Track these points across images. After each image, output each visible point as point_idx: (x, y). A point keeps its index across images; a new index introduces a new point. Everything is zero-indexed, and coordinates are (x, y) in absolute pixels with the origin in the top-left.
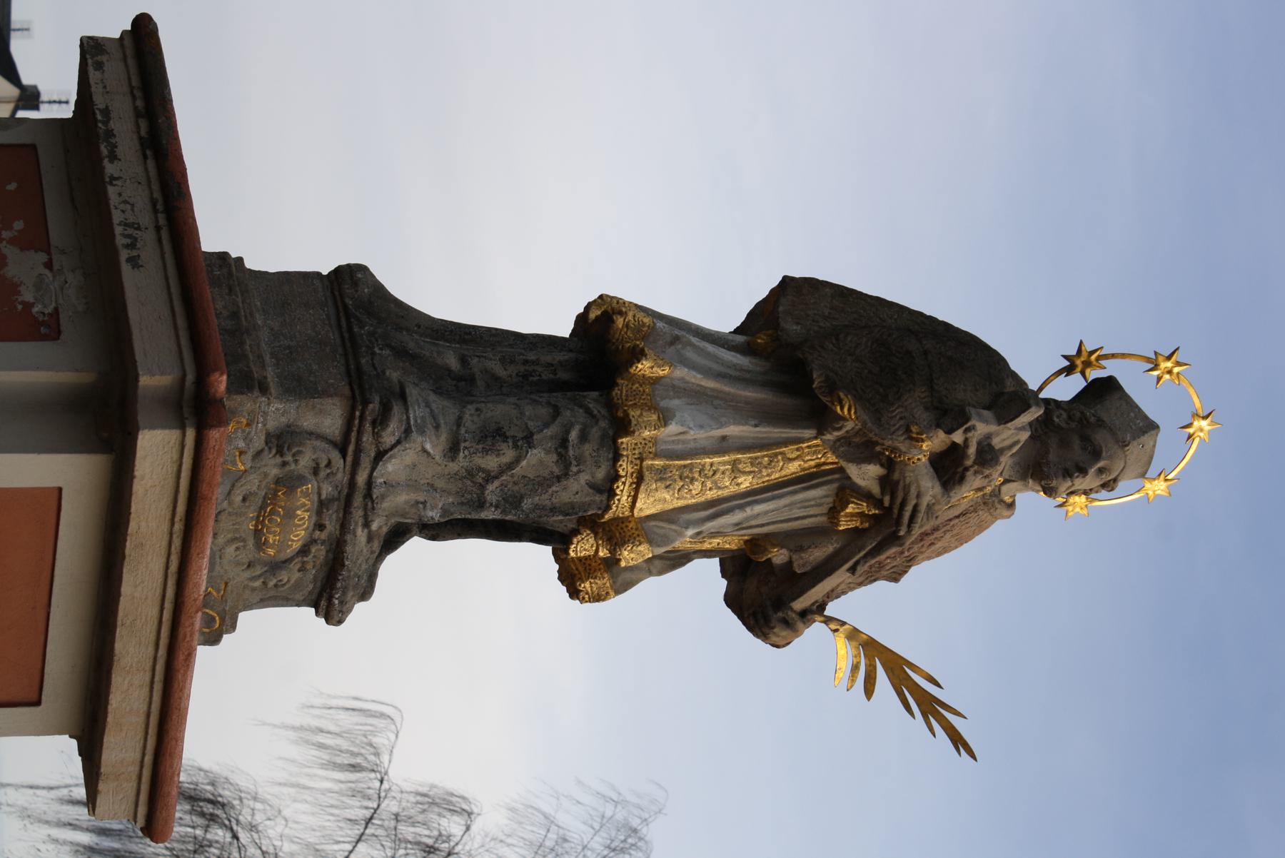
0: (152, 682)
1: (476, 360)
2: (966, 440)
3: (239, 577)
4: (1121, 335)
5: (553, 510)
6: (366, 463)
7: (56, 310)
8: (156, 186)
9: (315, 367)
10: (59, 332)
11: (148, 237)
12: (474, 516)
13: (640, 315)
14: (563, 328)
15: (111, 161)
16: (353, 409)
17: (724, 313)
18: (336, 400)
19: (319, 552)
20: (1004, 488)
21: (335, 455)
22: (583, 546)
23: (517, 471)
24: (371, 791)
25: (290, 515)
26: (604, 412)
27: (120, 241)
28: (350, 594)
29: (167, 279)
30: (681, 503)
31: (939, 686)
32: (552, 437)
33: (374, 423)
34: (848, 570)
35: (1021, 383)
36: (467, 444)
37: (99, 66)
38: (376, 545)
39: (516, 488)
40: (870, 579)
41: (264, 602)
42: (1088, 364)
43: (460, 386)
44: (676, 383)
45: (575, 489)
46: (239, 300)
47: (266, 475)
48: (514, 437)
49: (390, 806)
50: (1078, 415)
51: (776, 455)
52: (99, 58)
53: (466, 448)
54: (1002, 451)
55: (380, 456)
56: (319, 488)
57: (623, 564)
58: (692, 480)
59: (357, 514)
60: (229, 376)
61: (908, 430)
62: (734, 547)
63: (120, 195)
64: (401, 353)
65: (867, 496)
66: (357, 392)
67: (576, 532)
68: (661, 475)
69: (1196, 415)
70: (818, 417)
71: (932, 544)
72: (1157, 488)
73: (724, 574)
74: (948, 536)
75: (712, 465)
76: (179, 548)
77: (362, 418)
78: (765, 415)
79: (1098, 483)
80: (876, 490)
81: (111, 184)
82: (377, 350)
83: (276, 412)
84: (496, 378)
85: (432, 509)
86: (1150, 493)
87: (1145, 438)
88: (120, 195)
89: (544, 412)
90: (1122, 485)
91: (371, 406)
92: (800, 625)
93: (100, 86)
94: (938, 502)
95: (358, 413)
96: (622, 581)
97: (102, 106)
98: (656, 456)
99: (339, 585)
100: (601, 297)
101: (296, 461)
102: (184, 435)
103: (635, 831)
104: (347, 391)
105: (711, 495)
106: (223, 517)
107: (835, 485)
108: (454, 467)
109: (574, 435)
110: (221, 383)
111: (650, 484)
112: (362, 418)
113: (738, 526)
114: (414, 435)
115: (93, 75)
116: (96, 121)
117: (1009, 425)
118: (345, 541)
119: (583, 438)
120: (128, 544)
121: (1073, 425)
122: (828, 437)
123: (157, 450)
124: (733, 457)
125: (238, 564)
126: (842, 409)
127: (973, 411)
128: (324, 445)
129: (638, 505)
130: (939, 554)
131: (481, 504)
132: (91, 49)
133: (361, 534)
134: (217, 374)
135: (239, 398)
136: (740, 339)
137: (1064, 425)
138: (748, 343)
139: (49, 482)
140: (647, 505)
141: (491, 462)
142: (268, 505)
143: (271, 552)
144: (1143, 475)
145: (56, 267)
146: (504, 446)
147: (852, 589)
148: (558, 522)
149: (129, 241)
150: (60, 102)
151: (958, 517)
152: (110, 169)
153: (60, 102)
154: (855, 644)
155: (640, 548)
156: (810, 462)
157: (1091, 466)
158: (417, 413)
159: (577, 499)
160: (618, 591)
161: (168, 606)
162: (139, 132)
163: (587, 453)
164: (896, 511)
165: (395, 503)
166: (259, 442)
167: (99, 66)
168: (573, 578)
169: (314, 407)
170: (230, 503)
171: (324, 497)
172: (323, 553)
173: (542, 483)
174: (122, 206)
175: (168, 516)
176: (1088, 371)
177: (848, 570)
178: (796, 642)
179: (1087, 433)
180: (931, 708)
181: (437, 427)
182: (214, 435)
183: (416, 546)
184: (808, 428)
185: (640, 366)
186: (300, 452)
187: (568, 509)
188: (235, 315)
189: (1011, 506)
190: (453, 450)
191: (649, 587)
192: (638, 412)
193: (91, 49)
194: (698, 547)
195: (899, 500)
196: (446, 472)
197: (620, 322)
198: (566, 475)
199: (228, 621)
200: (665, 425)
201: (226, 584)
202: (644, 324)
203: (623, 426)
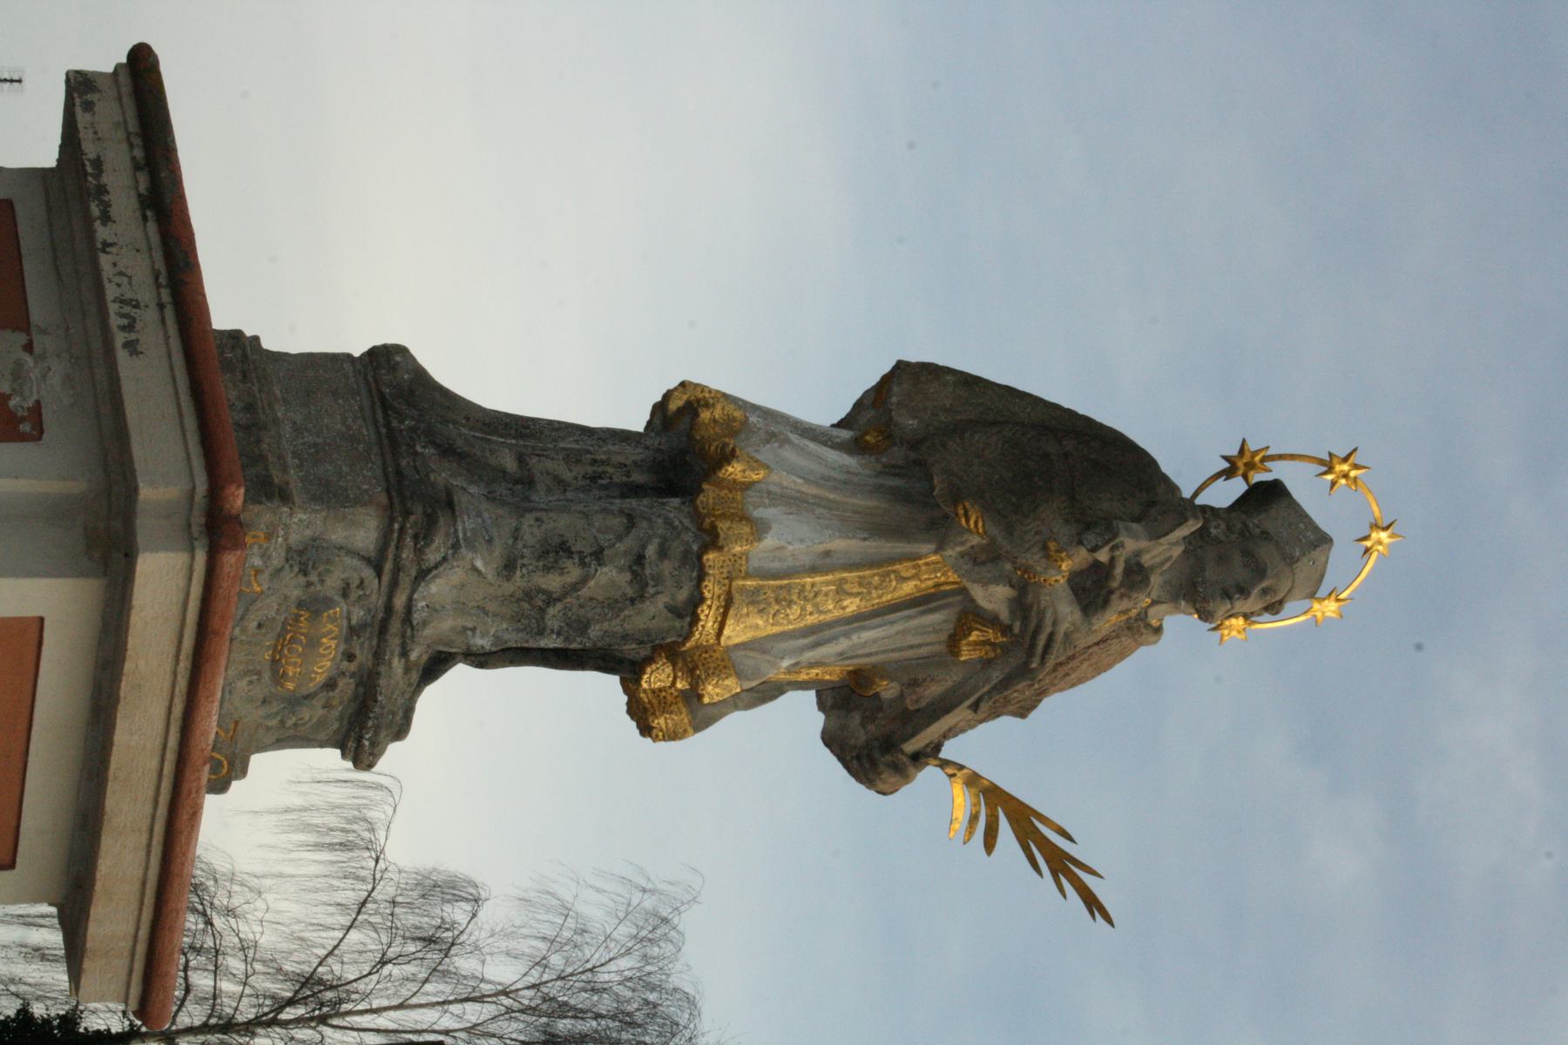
0: (149, 845)
1: (535, 460)
2: (1112, 559)
3: (252, 715)
4: (1289, 433)
5: (625, 637)
6: (405, 581)
7: (38, 403)
8: (158, 256)
9: (345, 469)
10: (41, 432)
11: (149, 316)
12: (532, 644)
13: (730, 408)
14: (637, 421)
15: (104, 224)
16: (392, 520)
17: (826, 403)
18: (371, 510)
19: (346, 686)
20: (1152, 611)
21: (368, 573)
22: (657, 677)
23: (584, 592)
24: (363, 873)
25: (313, 643)
26: (687, 522)
27: (115, 321)
28: (383, 734)
29: (172, 369)
30: (776, 629)
31: (1071, 839)
32: (625, 553)
33: (416, 537)
34: (969, 707)
35: (1173, 488)
36: (525, 561)
37: (89, 107)
38: (415, 676)
39: (582, 611)
40: (994, 714)
41: (281, 743)
42: (1251, 466)
43: (518, 489)
44: (773, 488)
45: (652, 614)
46: (256, 388)
47: (286, 598)
48: (581, 552)
49: (385, 891)
50: (1239, 526)
51: (888, 574)
52: (89, 97)
53: (524, 565)
54: (1152, 568)
55: (423, 575)
56: (349, 613)
57: (706, 700)
58: (790, 603)
59: (394, 642)
60: (247, 490)
61: (1045, 548)
62: (835, 678)
63: (115, 265)
64: (448, 451)
65: (992, 620)
66: (396, 501)
67: (650, 660)
68: (754, 598)
69: (1375, 526)
70: (939, 528)
71: (1067, 675)
72: (1330, 608)
73: (821, 706)
74: (1086, 664)
75: (813, 585)
76: (184, 690)
77: (402, 530)
78: (880, 529)
79: (1260, 605)
80: (1004, 615)
81: (104, 251)
82: (419, 449)
83: (300, 523)
84: (559, 481)
85: (482, 637)
86: (1319, 615)
87: (1316, 554)
88: (115, 265)
89: (617, 522)
90: (1289, 607)
91: (412, 518)
92: (911, 770)
93: (90, 131)
94: (1077, 630)
95: (396, 526)
96: (701, 716)
97: (92, 156)
98: (747, 576)
99: (370, 723)
100: (683, 384)
101: (322, 582)
102: (193, 558)
103: (665, 920)
104: (384, 499)
105: (811, 620)
106: (236, 644)
107: (957, 609)
108: (509, 588)
109: (651, 551)
110: (237, 497)
111: (740, 607)
112: (402, 530)
113: (842, 655)
114: (463, 550)
115: (82, 118)
116: (86, 174)
117: (1162, 540)
118: (378, 674)
119: (663, 553)
120: (123, 685)
121: (1234, 537)
122: (949, 552)
123: (162, 579)
124: (839, 575)
125: (251, 700)
126: (968, 521)
127: (1121, 525)
128: (356, 562)
129: (726, 632)
130: (1073, 685)
131: (541, 632)
132: (80, 85)
133: (397, 665)
134: (233, 488)
135: (256, 508)
136: (845, 434)
137: (1222, 537)
138: (856, 440)
139: (29, 610)
140: (734, 633)
141: (553, 582)
142: (287, 632)
143: (290, 686)
144: (1312, 595)
145: (37, 349)
146: (568, 563)
147: (972, 727)
148: (630, 650)
149: (125, 322)
150: (12, 81)
151: (1097, 644)
152: (102, 233)
153: (12, 81)
154: (974, 790)
155: (727, 682)
156: (927, 582)
157: (1254, 585)
158: (466, 524)
159: (653, 625)
160: (698, 728)
161: (171, 757)
162: (137, 188)
163: (667, 573)
164: (1028, 640)
165: (439, 629)
166: (277, 560)
167: (89, 107)
168: (643, 714)
169: (344, 518)
170: (243, 630)
171: (354, 622)
172: (353, 686)
173: (614, 605)
174: (117, 279)
175: (172, 650)
176: (1251, 474)
177: (969, 707)
178: (905, 790)
179: (1251, 544)
180: (1061, 865)
181: (490, 541)
182: (229, 560)
183: (460, 673)
184: (929, 541)
185: (730, 469)
186: (329, 571)
187: (643, 638)
188: (250, 408)
189: (1158, 630)
190: (509, 567)
191: (734, 722)
192: (728, 524)
193: (80, 85)
194: (792, 677)
195: (1032, 626)
196: (500, 592)
197: (705, 415)
198: (642, 597)
199: (238, 766)
200: (760, 539)
201: (236, 723)
202: (734, 419)
203: (712, 540)
